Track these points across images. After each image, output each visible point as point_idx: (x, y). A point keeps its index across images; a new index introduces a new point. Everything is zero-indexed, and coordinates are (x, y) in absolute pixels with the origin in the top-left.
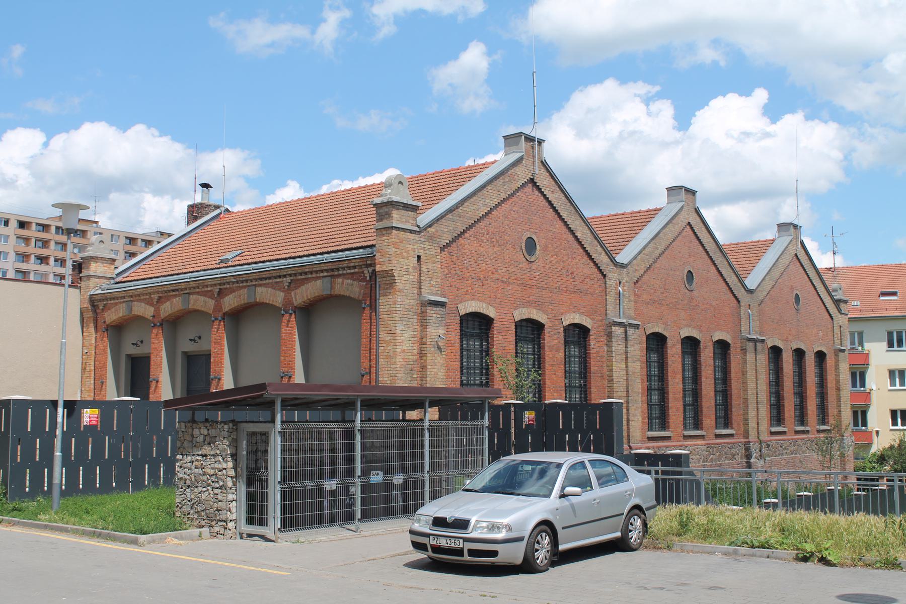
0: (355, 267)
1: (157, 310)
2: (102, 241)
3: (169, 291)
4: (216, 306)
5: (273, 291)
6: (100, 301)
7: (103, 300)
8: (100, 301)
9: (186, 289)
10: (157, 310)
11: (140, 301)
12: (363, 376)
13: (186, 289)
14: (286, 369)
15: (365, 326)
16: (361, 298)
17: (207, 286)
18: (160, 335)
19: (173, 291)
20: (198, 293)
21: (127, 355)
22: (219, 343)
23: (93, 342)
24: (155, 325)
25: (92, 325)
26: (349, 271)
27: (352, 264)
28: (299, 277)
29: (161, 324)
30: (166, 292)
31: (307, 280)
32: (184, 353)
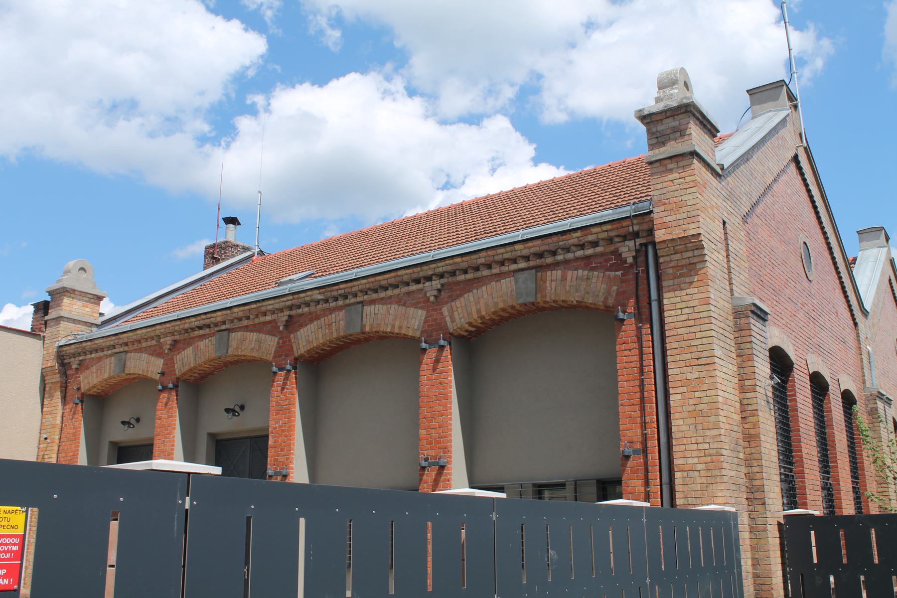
0: (595, 244)
1: (169, 364)
2: (82, 269)
3: (193, 329)
4: (279, 347)
5: (402, 309)
6: (74, 355)
7: (79, 354)
8: (74, 355)
9: (224, 323)
10: (169, 364)
11: (140, 350)
12: (627, 457)
13: (224, 323)
14: (432, 453)
15: (626, 358)
16: (611, 302)
17: (265, 314)
18: (174, 404)
19: (200, 328)
20: (246, 328)
21: (111, 442)
22: (287, 411)
23: (58, 421)
24: (165, 388)
25: (58, 394)
26: (580, 253)
27: (591, 238)
28: (461, 277)
29: (176, 386)
30: (186, 331)
31: (478, 282)
32: (212, 436)
